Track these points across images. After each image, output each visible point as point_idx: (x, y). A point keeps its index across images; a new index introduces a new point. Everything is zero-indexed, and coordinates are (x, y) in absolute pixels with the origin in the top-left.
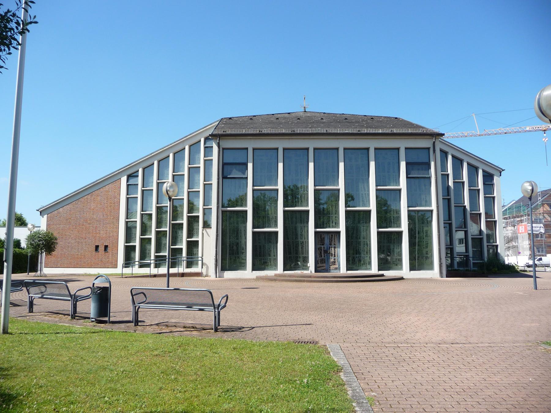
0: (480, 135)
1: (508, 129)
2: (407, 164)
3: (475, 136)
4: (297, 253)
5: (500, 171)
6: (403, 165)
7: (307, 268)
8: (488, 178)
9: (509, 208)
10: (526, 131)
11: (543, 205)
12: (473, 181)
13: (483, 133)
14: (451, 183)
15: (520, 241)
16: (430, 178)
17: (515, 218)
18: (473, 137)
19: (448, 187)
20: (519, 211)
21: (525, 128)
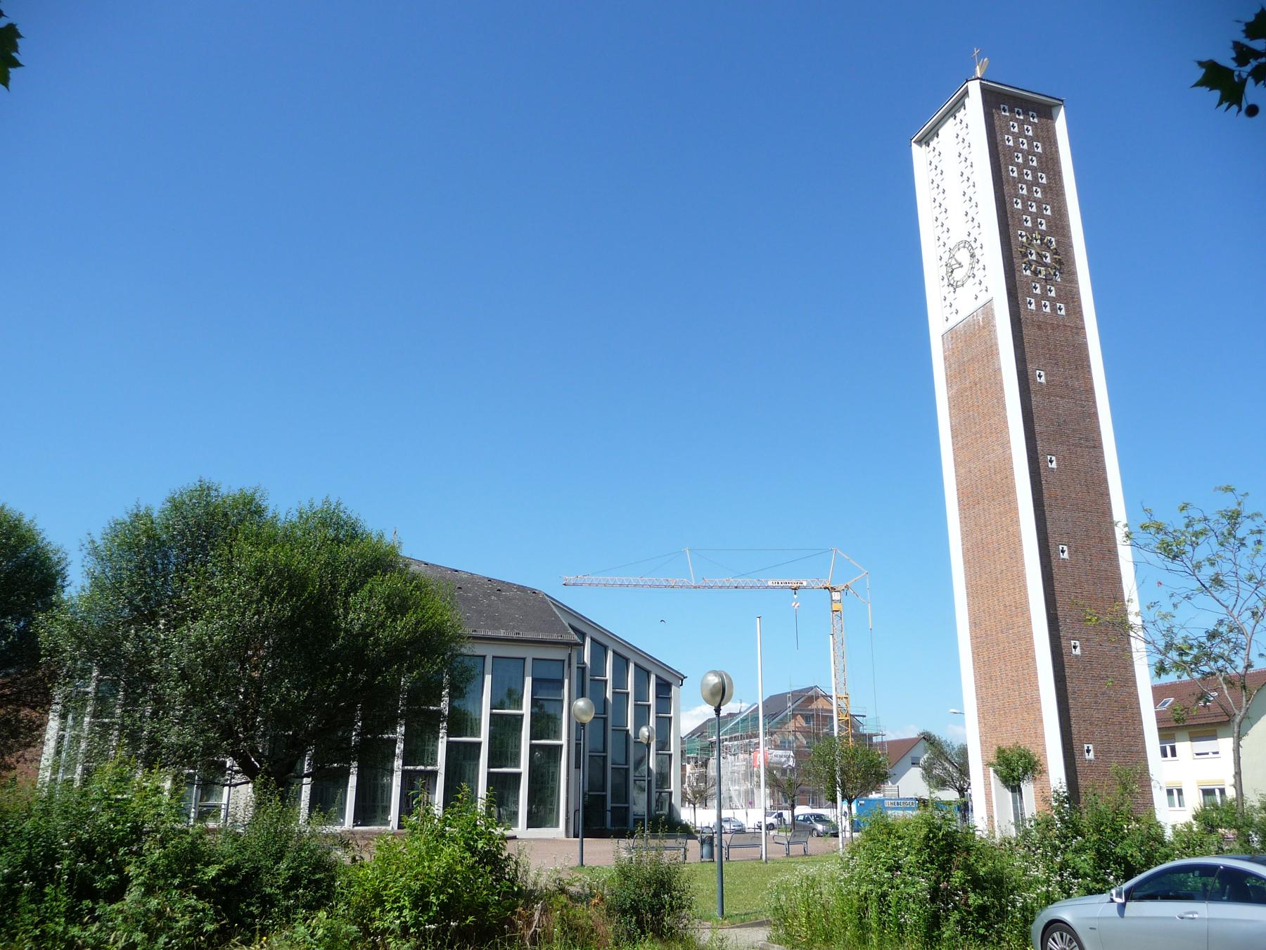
1: (740, 581)
2: (535, 681)
3: (688, 587)
4: (374, 800)
5: (681, 678)
6: (528, 681)
7: (387, 823)
8: (664, 688)
9: (743, 720)
11: (794, 716)
12: (641, 693)
13: (701, 583)
14: (609, 695)
16: (562, 701)
18: (684, 589)
19: (606, 700)
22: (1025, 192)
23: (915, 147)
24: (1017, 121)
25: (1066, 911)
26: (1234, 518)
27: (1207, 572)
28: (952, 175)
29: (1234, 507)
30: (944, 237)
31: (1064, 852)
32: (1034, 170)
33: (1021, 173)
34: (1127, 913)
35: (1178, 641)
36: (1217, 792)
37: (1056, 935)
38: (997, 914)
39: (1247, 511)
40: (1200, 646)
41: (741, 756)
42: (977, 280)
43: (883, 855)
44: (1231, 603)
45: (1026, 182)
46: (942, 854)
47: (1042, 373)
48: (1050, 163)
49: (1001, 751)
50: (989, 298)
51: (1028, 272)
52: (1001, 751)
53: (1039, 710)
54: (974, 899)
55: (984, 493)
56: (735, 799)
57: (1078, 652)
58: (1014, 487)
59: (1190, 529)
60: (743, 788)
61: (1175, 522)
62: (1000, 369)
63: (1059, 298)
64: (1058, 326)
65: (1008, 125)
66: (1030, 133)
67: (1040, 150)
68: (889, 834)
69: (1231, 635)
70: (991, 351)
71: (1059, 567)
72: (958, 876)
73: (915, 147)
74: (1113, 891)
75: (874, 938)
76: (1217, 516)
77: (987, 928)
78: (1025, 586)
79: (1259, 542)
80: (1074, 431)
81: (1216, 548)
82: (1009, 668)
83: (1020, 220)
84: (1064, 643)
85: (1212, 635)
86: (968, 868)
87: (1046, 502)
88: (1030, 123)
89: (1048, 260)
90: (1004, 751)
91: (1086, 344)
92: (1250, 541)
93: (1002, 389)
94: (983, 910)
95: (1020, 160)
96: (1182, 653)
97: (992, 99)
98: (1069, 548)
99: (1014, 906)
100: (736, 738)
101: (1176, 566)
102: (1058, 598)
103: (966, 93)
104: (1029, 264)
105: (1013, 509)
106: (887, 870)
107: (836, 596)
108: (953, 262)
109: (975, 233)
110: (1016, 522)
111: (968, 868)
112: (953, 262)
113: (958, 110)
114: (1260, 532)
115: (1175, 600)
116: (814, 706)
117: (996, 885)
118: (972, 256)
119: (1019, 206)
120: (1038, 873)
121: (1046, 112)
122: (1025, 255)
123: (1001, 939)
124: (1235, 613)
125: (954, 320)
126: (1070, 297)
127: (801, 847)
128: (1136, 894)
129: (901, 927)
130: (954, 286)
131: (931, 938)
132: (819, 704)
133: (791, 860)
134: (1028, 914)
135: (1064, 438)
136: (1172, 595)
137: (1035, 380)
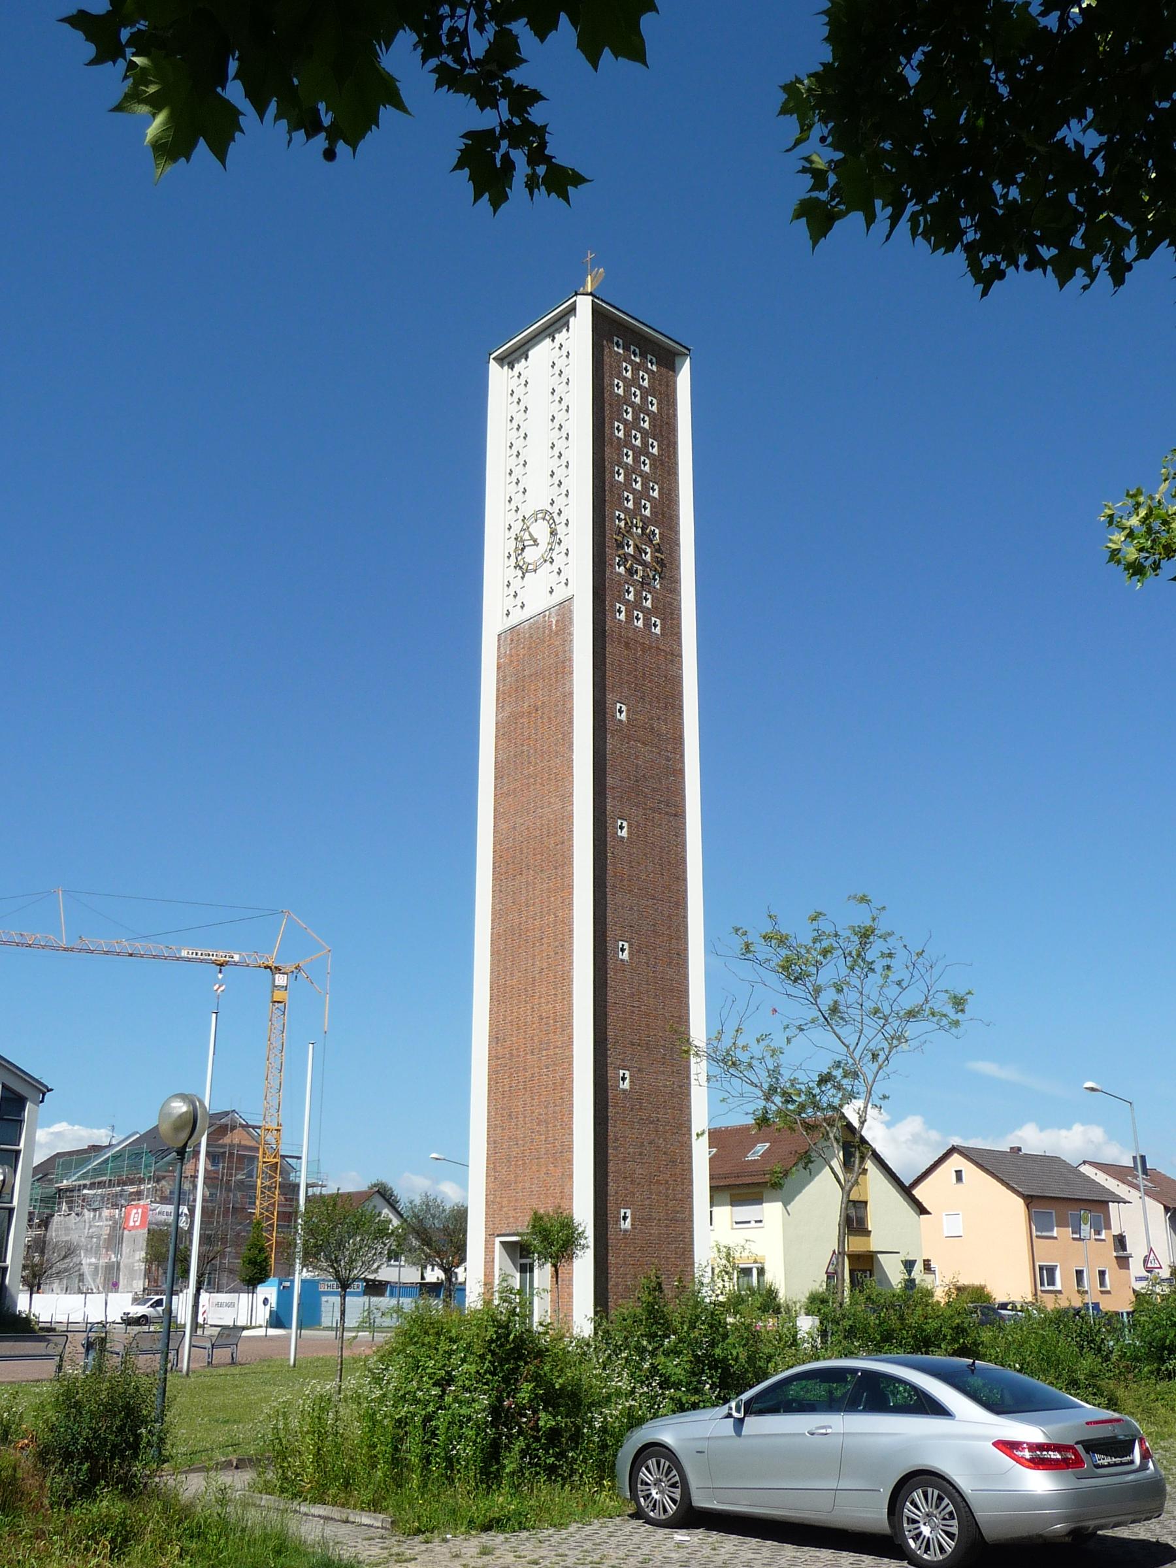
0: (66, 950)
1: (139, 946)
3: (54, 948)
5: (42, 1090)
9: (115, 1157)
10: (178, 959)
13: (77, 944)
15: (126, 1249)
17: (125, 1184)
18: (47, 951)
20: (136, 1167)
21: (180, 950)
22: (630, 460)
23: (493, 365)
24: (631, 362)
25: (669, 1432)
26: (865, 935)
27: (827, 998)
28: (539, 413)
29: (868, 923)
30: (518, 499)
31: (653, 1354)
32: (645, 434)
33: (628, 434)
34: (745, 1431)
35: (784, 1082)
36: (755, 1272)
37: (652, 1463)
38: (571, 1438)
39: (882, 927)
40: (809, 1093)
41: (106, 1213)
42: (555, 567)
43: (431, 1363)
44: (851, 1040)
45: (633, 447)
46: (508, 1361)
47: (624, 708)
48: (665, 429)
49: (537, 1218)
50: (570, 594)
51: (622, 570)
52: (537, 1218)
53: (570, 1161)
54: (545, 1420)
55: (530, 860)
56: (88, 1278)
57: (626, 1085)
58: (571, 857)
59: (818, 945)
60: (103, 1261)
61: (802, 934)
62: (571, 694)
63: (655, 611)
64: (651, 647)
65: (620, 366)
66: (646, 384)
67: (654, 409)
68: (438, 1334)
69: (844, 1082)
70: (564, 668)
71: (616, 971)
72: (525, 1391)
73: (493, 365)
74: (733, 1404)
75: (415, 1479)
76: (848, 933)
77: (558, 1456)
78: (570, 994)
79: (888, 967)
80: (654, 790)
81: (844, 971)
82: (535, 1102)
83: (620, 497)
84: (611, 1072)
85: (824, 1080)
86: (537, 1378)
87: (610, 881)
88: (647, 370)
89: (648, 558)
90: (541, 1218)
91: (680, 677)
92: (878, 967)
93: (571, 722)
94: (554, 1434)
95: (629, 417)
96: (789, 1100)
97: (606, 327)
98: (631, 946)
99: (591, 1427)
100: (101, 1185)
101: (798, 990)
102: (610, 1013)
103: (572, 310)
104: (625, 558)
105: (567, 887)
106: (434, 1385)
107: (281, 980)
108: (526, 536)
109: (560, 502)
110: (568, 904)
111: (537, 1378)
112: (526, 536)
113: (559, 331)
114: (890, 955)
115: (789, 1033)
116: (226, 1140)
117: (570, 1400)
118: (553, 533)
119: (621, 478)
120: (622, 1383)
121: (668, 360)
122: (620, 546)
123: (573, 1472)
124: (857, 1055)
125: (518, 616)
126: (669, 612)
127: (227, 1352)
128: (756, 1406)
129: (450, 1462)
130: (523, 569)
131: (488, 1474)
132: (235, 1138)
133: (215, 1372)
134: (611, 1439)
135: (641, 799)
136: (787, 1027)
137: (614, 716)
